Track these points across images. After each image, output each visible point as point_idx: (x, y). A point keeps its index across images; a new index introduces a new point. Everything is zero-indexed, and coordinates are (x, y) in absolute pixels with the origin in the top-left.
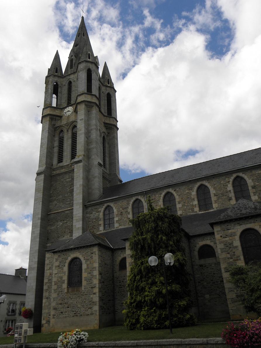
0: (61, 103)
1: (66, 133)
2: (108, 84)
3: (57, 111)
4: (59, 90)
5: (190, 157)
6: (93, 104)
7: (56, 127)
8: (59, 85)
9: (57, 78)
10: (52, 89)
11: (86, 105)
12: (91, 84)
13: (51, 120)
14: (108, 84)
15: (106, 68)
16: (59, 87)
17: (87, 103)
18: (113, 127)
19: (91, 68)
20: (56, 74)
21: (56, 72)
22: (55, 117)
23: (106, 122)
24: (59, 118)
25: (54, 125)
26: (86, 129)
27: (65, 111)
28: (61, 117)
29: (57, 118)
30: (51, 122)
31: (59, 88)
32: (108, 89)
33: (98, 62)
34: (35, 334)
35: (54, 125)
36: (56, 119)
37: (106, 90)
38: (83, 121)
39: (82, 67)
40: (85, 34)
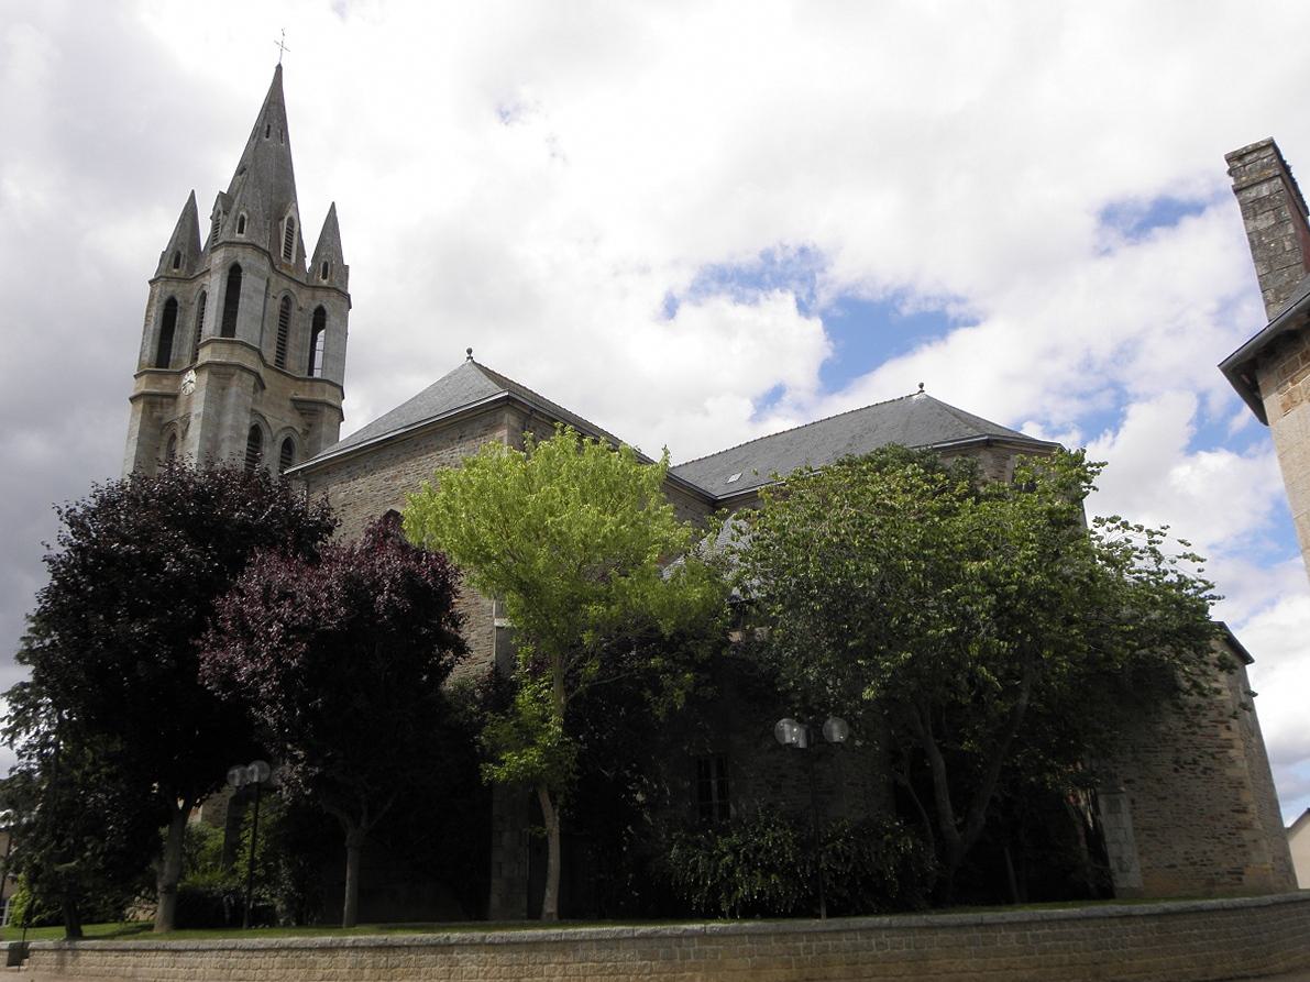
0: (179, 355)
1: (180, 444)
2: (325, 277)
3: (165, 382)
4: (178, 319)
5: (1157, 230)
6: (232, 370)
7: (167, 424)
8: (179, 305)
9: (175, 284)
10: (160, 317)
11: (212, 373)
12: (237, 307)
13: (152, 407)
14: (325, 277)
15: (331, 226)
16: (179, 309)
17: (215, 369)
18: (319, 408)
19: (240, 261)
20: (175, 271)
21: (176, 266)
22: (159, 399)
23: (301, 396)
24: (170, 400)
25: (160, 419)
26: (208, 440)
27: (184, 382)
28: (175, 397)
29: (165, 400)
30: (151, 413)
31: (178, 313)
32: (319, 294)
33: (296, 218)
34: (1116, 893)
35: (160, 419)
36: (162, 404)
37: (313, 298)
38: (201, 419)
39: (217, 262)
40: (272, 129)
